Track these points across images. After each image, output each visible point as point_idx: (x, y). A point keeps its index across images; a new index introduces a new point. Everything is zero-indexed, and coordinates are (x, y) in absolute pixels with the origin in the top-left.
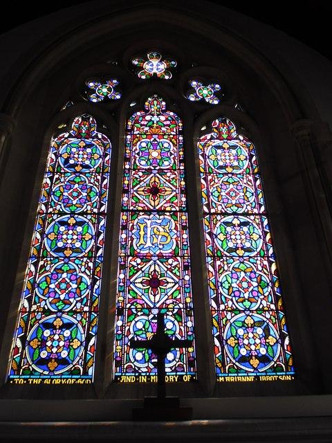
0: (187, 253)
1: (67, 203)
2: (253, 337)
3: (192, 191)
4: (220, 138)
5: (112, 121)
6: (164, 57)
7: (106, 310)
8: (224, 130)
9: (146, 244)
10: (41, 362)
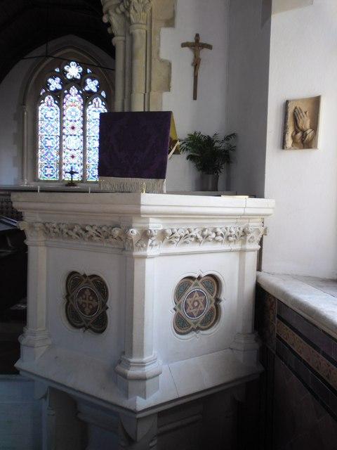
0: (82, 148)
1: (46, 131)
2: (106, 111)
3: (84, 128)
4: (95, 107)
5: (59, 96)
6: (79, 64)
7: (60, 164)
8: (97, 103)
9: (71, 146)
10: (47, 175)
